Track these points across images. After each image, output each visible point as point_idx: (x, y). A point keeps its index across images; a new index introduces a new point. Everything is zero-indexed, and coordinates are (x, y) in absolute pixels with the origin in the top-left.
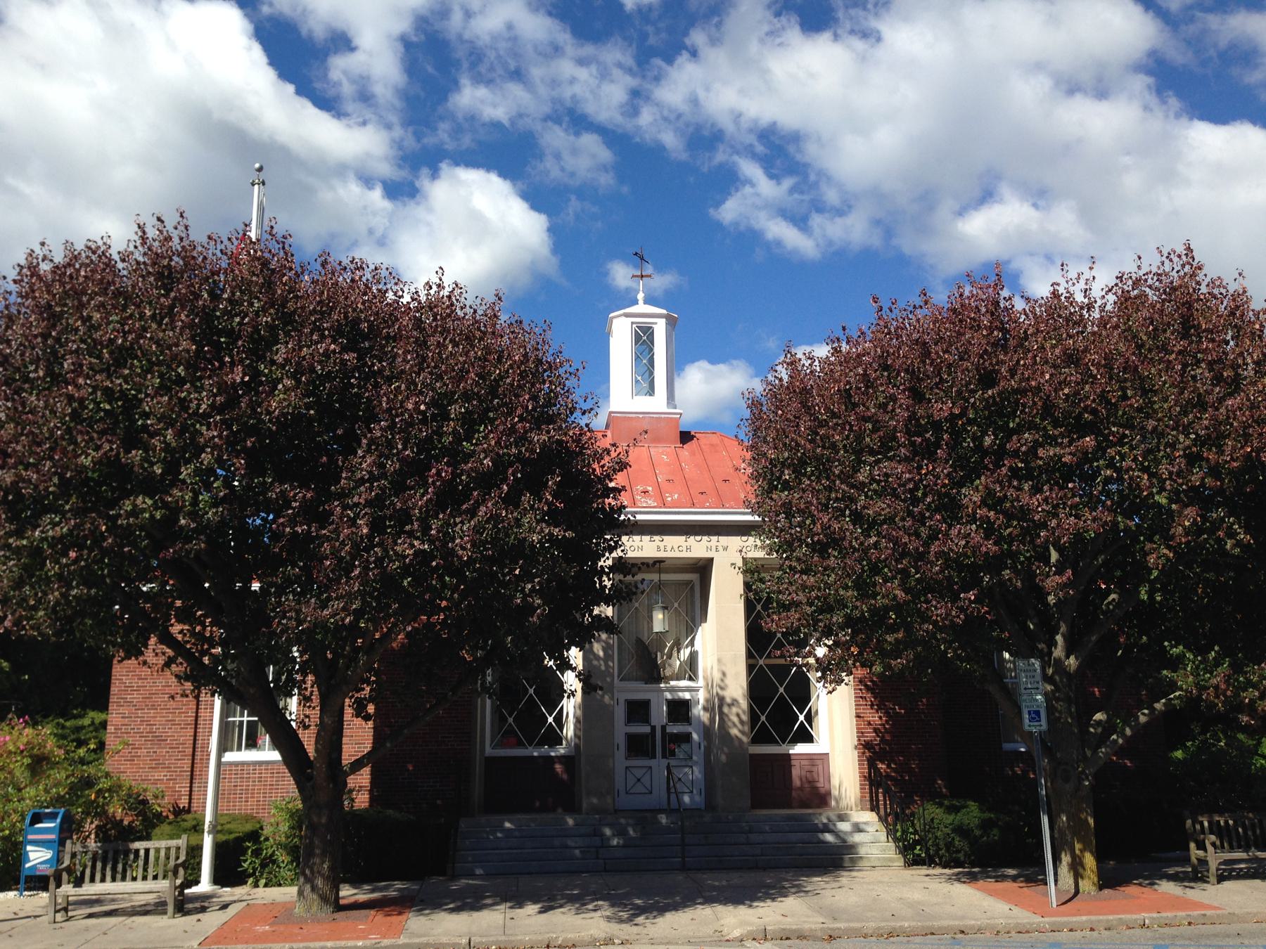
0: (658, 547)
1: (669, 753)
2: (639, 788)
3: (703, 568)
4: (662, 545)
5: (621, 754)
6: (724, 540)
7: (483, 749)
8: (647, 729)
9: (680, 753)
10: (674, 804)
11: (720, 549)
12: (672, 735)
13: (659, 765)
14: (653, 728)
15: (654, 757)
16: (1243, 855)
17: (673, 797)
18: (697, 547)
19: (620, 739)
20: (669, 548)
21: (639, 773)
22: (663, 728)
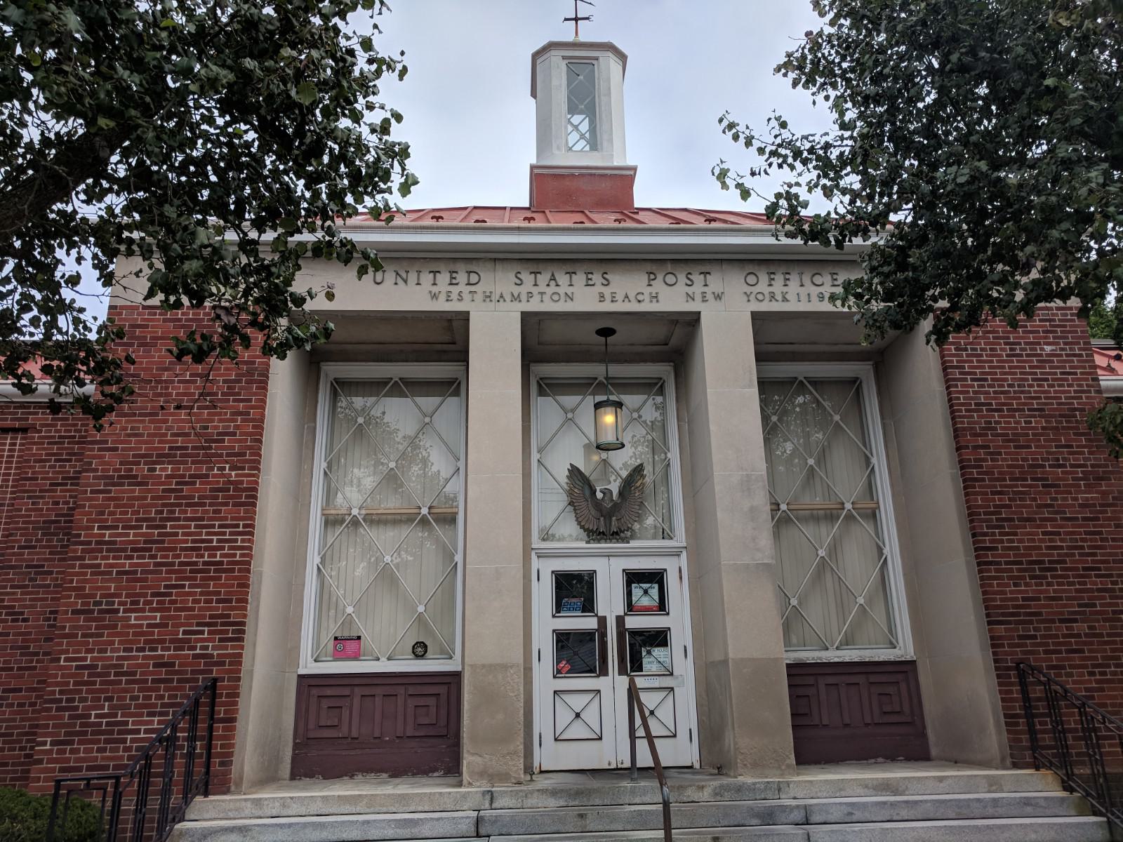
0: (602, 296)
1: (632, 664)
2: (578, 731)
3: (687, 325)
4: (607, 291)
5: (543, 670)
6: (716, 281)
7: (290, 651)
8: (589, 623)
9: (649, 664)
10: (644, 759)
11: (709, 296)
12: (635, 633)
13: (614, 685)
14: (602, 621)
15: (604, 672)
16: (760, 780)
17: (642, 745)
18: (670, 297)
19: (544, 643)
20: (620, 297)
21: (565, 717)
22: (620, 621)
